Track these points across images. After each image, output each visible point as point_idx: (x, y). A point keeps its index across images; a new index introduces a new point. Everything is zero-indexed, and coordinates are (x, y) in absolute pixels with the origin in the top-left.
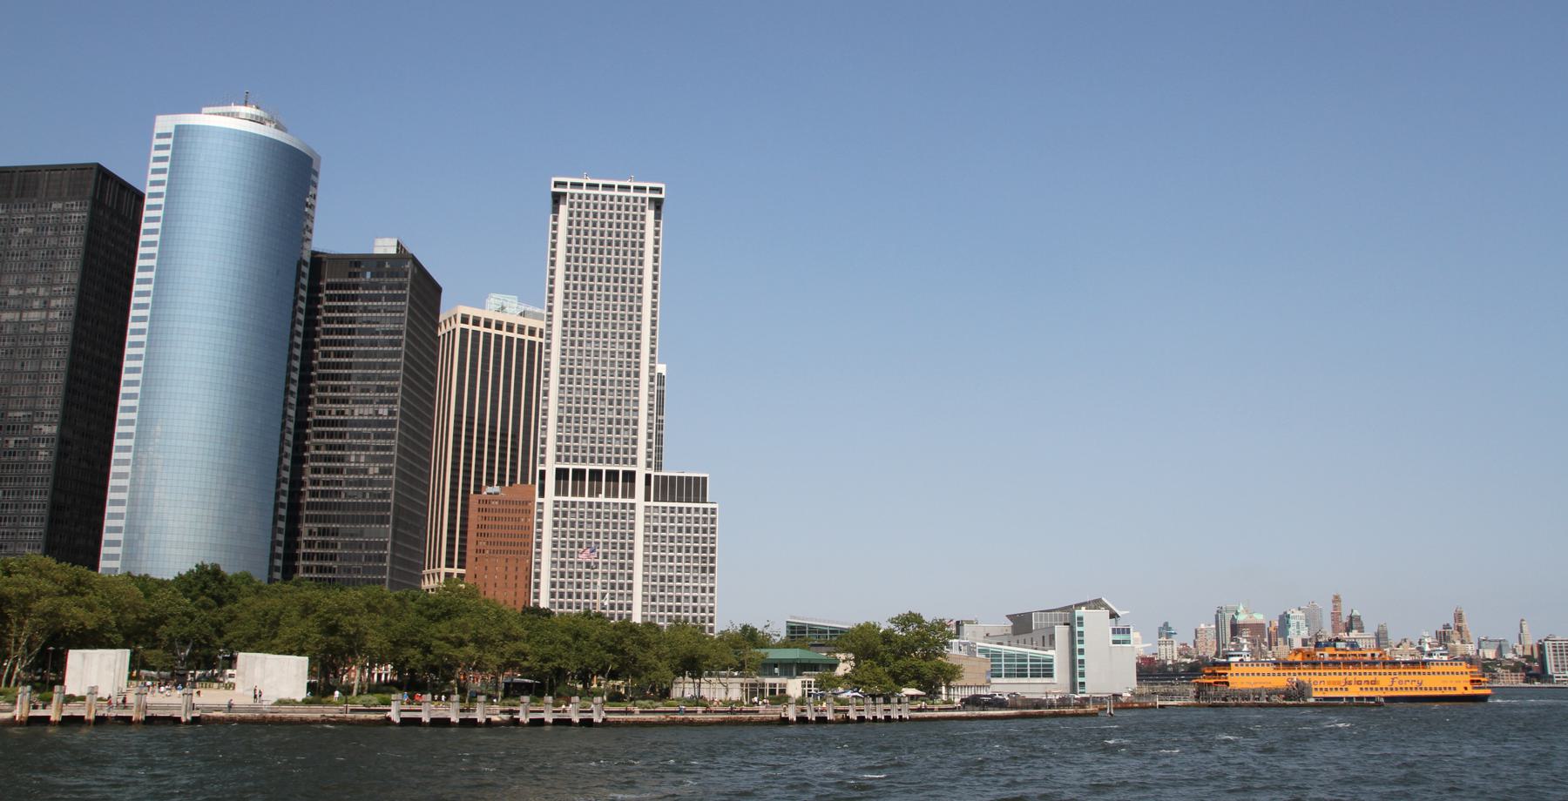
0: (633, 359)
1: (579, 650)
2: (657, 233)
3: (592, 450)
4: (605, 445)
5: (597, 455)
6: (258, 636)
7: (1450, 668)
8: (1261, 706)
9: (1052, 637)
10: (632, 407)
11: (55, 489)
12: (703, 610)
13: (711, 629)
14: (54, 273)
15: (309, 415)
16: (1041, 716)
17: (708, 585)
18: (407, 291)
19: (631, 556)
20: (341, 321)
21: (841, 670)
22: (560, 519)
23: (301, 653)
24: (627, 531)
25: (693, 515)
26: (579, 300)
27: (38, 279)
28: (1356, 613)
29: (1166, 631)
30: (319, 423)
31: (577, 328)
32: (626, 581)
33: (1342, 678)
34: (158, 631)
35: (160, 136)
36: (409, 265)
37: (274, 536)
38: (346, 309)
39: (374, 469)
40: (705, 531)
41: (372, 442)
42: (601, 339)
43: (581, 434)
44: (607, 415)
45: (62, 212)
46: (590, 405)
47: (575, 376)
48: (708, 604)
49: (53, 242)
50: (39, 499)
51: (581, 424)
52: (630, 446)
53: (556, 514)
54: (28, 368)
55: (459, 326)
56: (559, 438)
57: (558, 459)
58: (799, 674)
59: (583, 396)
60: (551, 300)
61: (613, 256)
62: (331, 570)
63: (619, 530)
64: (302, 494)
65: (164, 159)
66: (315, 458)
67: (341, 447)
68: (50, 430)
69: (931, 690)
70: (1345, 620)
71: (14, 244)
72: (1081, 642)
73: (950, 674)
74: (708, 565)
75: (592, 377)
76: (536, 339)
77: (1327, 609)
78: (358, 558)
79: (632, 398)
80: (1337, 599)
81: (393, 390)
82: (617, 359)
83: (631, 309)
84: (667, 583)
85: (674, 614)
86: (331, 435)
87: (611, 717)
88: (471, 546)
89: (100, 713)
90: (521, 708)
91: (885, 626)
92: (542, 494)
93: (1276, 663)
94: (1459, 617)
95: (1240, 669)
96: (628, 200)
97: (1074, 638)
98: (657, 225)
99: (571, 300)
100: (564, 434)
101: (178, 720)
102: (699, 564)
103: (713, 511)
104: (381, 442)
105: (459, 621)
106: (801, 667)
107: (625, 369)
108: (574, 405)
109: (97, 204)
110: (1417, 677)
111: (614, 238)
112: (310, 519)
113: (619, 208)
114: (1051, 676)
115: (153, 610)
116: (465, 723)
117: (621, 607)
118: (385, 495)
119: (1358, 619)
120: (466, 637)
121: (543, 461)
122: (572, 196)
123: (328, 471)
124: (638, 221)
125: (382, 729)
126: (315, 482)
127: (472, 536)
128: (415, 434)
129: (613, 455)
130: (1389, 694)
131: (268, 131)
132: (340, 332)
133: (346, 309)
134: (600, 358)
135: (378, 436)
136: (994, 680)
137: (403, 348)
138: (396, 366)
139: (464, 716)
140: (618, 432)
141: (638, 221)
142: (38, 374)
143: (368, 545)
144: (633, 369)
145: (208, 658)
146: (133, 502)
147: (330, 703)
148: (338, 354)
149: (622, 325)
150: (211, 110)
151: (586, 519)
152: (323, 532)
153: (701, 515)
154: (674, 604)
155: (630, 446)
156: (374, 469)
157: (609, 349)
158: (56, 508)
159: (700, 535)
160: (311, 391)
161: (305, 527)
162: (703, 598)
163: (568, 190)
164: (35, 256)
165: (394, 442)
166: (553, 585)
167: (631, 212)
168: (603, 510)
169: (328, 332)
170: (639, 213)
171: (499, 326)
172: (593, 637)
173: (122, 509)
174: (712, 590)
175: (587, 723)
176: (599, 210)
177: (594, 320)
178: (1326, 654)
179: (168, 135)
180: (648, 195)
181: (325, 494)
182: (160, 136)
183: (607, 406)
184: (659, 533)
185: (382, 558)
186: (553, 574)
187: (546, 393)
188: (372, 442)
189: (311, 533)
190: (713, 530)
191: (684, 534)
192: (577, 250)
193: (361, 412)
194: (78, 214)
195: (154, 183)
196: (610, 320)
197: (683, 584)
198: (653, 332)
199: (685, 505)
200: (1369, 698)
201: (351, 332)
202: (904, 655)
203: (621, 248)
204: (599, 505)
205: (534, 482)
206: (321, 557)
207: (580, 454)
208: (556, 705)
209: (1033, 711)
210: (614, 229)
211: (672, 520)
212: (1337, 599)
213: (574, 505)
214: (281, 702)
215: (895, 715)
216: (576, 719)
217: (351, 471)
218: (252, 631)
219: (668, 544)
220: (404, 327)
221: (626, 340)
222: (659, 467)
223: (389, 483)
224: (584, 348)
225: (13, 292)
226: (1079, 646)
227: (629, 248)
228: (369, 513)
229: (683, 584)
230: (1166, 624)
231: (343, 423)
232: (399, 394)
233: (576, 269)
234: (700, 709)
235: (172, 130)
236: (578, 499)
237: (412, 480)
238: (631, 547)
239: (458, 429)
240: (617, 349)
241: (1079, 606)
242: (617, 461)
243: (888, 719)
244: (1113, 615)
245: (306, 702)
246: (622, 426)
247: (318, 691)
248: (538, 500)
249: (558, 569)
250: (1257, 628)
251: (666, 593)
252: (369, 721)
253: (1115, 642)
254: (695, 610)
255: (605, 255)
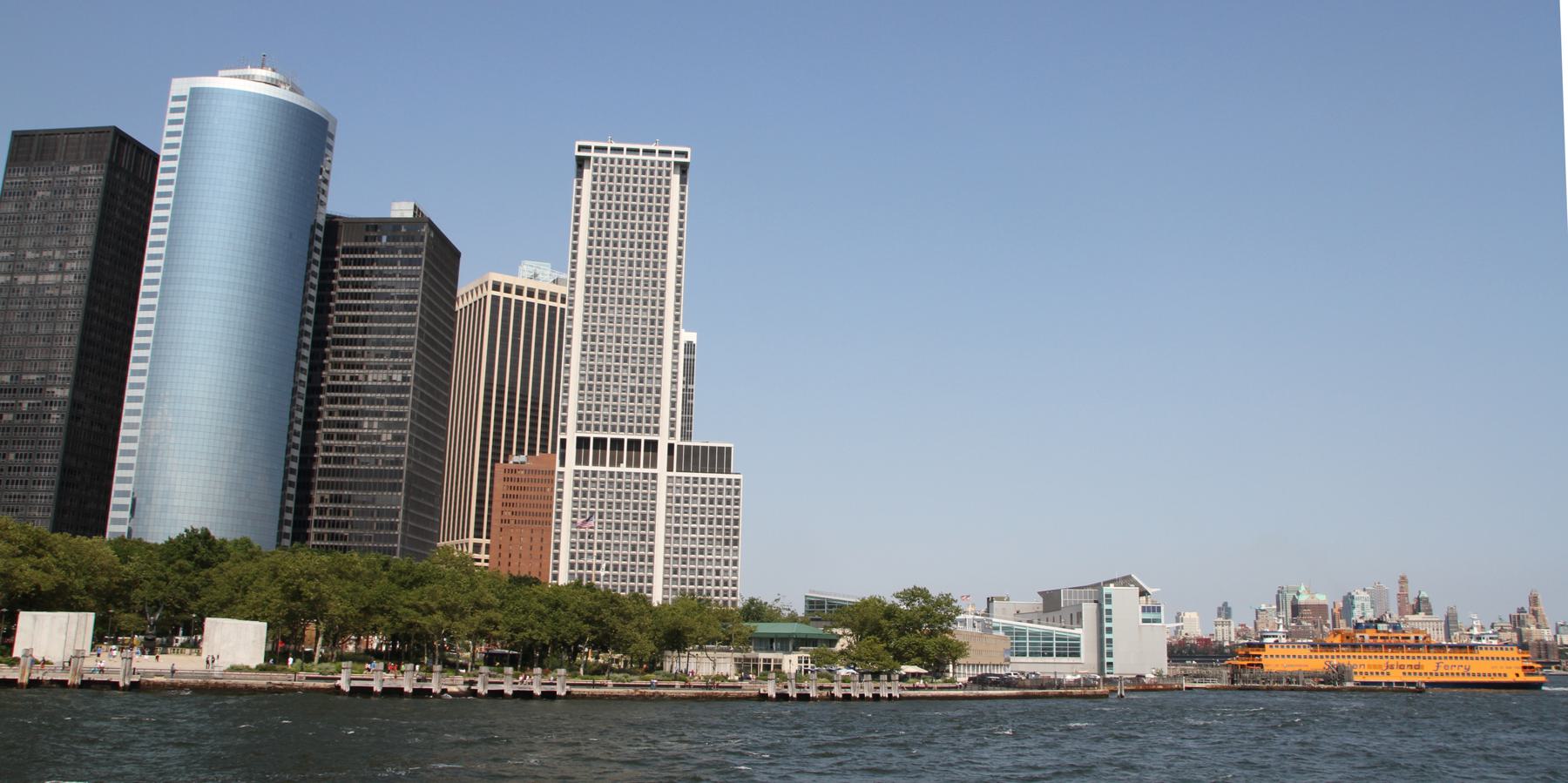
0: (657, 326)
1: (556, 620)
2: (682, 198)
3: (614, 418)
4: (627, 414)
5: (618, 423)
6: (231, 601)
7: (1499, 653)
8: (1293, 689)
9: (1080, 615)
10: (655, 375)
11: (66, 452)
12: (726, 584)
13: (734, 603)
14: (70, 236)
15: (323, 380)
16: (1045, 696)
17: (731, 557)
18: (423, 256)
19: (652, 528)
20: (356, 285)
21: (842, 644)
22: (581, 488)
23: (263, 619)
24: (649, 501)
25: (717, 486)
26: (602, 266)
27: (55, 242)
28: (1424, 594)
29: (1225, 611)
30: (332, 388)
31: (600, 295)
32: (647, 553)
33: (1383, 662)
34: (132, 595)
35: (176, 99)
36: (425, 229)
37: (283, 502)
38: (362, 273)
39: (387, 436)
40: (728, 502)
41: (386, 408)
42: (625, 305)
43: (602, 402)
44: (629, 383)
45: (79, 175)
46: (612, 373)
47: (597, 343)
48: (731, 578)
49: (70, 205)
50: (50, 462)
51: (603, 392)
52: (653, 415)
53: (576, 484)
54: (42, 330)
55: (490, 293)
56: (581, 406)
57: (579, 427)
58: (795, 649)
59: (605, 363)
60: (574, 265)
61: (637, 221)
62: (343, 538)
63: (640, 501)
64: (315, 460)
65: (179, 122)
66: (328, 424)
67: (356, 413)
68: (62, 393)
69: (937, 669)
70: (1412, 602)
71: (33, 207)
72: (1109, 620)
73: (954, 652)
74: (732, 537)
75: (614, 344)
76: (558, 305)
77: (1394, 590)
78: (370, 526)
79: (656, 365)
80: (1403, 580)
81: (408, 355)
82: (640, 326)
83: (655, 275)
84: (689, 556)
85: (679, 586)
86: (344, 401)
87: (576, 690)
88: (496, 516)
89: (34, 676)
90: (478, 679)
91: (890, 599)
92: (562, 464)
93: (1313, 645)
94: (1534, 600)
95: (1275, 651)
96: (652, 164)
97: (1102, 616)
98: (683, 189)
99: (594, 265)
100: (585, 402)
101: (115, 685)
102: (723, 537)
103: (738, 482)
104: (395, 408)
105: (428, 587)
106: (799, 642)
107: (648, 336)
108: (596, 372)
109: (113, 167)
110: (1464, 662)
111: (638, 203)
112: (322, 486)
113: (644, 172)
114: (1078, 655)
115: (127, 574)
116: (420, 693)
117: (641, 579)
118: (398, 462)
119: (1426, 601)
120: (434, 605)
121: (564, 429)
122: (596, 160)
123: (341, 437)
124: (663, 186)
125: (332, 698)
126: (328, 448)
127: (497, 505)
128: (429, 401)
129: (635, 424)
130: (1434, 679)
131: (283, 94)
132: (355, 296)
133: (362, 273)
134: (623, 325)
135: (391, 402)
136: (1013, 659)
137: (417, 313)
138: (411, 331)
139: (419, 686)
140: (640, 400)
141: (663, 186)
142: (51, 338)
143: (380, 513)
144: (656, 336)
145: (179, 625)
146: (141, 466)
147: (283, 670)
148: (354, 319)
149: (646, 291)
150: (232, 72)
151: (606, 489)
152: (337, 499)
153: (725, 486)
154: (697, 577)
155: (653, 415)
156: (387, 436)
157: (632, 316)
158: (66, 471)
159: (724, 506)
160: (325, 356)
161: (317, 494)
162: (726, 572)
163: (592, 154)
164: (51, 219)
165: (407, 409)
166: (572, 556)
167: (656, 176)
168: (624, 480)
169: (343, 296)
170: (664, 177)
171: (531, 294)
172: (572, 607)
173: (131, 473)
174: (735, 563)
175: (550, 696)
176: (624, 174)
177: (617, 286)
178: (1367, 635)
179: (183, 98)
180: (673, 159)
181: (337, 460)
182: (176, 99)
183: (630, 374)
184: (682, 504)
185: (393, 526)
186: (573, 546)
187: (568, 360)
188: (386, 408)
189: (322, 500)
190: (737, 502)
191: (707, 505)
192: (601, 215)
193: (375, 378)
194: (94, 177)
195: (168, 146)
196: (634, 286)
197: (706, 556)
198: (678, 299)
199: (708, 476)
200: (1409, 684)
201: (367, 296)
202: (907, 631)
203: (646, 212)
204: (620, 475)
205: (554, 451)
206: (333, 524)
207: (601, 423)
208: (545, 674)
209: (1046, 689)
210: (639, 193)
211: (695, 491)
212: (1403, 580)
213: (594, 474)
214: (234, 669)
215: (884, 693)
216: (538, 692)
217: (363, 438)
218: (225, 597)
219: (690, 515)
220: (419, 291)
221: (649, 306)
222: (686, 435)
223: (402, 450)
224: (607, 314)
225: (30, 255)
226: (1106, 625)
227: (654, 213)
228: (383, 480)
229: (706, 556)
230: (1225, 604)
231: (359, 389)
232: (413, 360)
233: (600, 234)
234: (677, 683)
235: (187, 93)
236: (599, 468)
237: (425, 447)
238: (653, 518)
239: (488, 397)
240: (641, 316)
241: (1107, 583)
242: (639, 430)
243: (876, 697)
244: (1143, 593)
245: (260, 669)
246: (645, 394)
247: (276, 656)
248: (558, 469)
249: (578, 540)
250: (1321, 609)
251: (688, 566)
252: (318, 690)
253: (1145, 621)
254: (717, 583)
255: (629, 220)
